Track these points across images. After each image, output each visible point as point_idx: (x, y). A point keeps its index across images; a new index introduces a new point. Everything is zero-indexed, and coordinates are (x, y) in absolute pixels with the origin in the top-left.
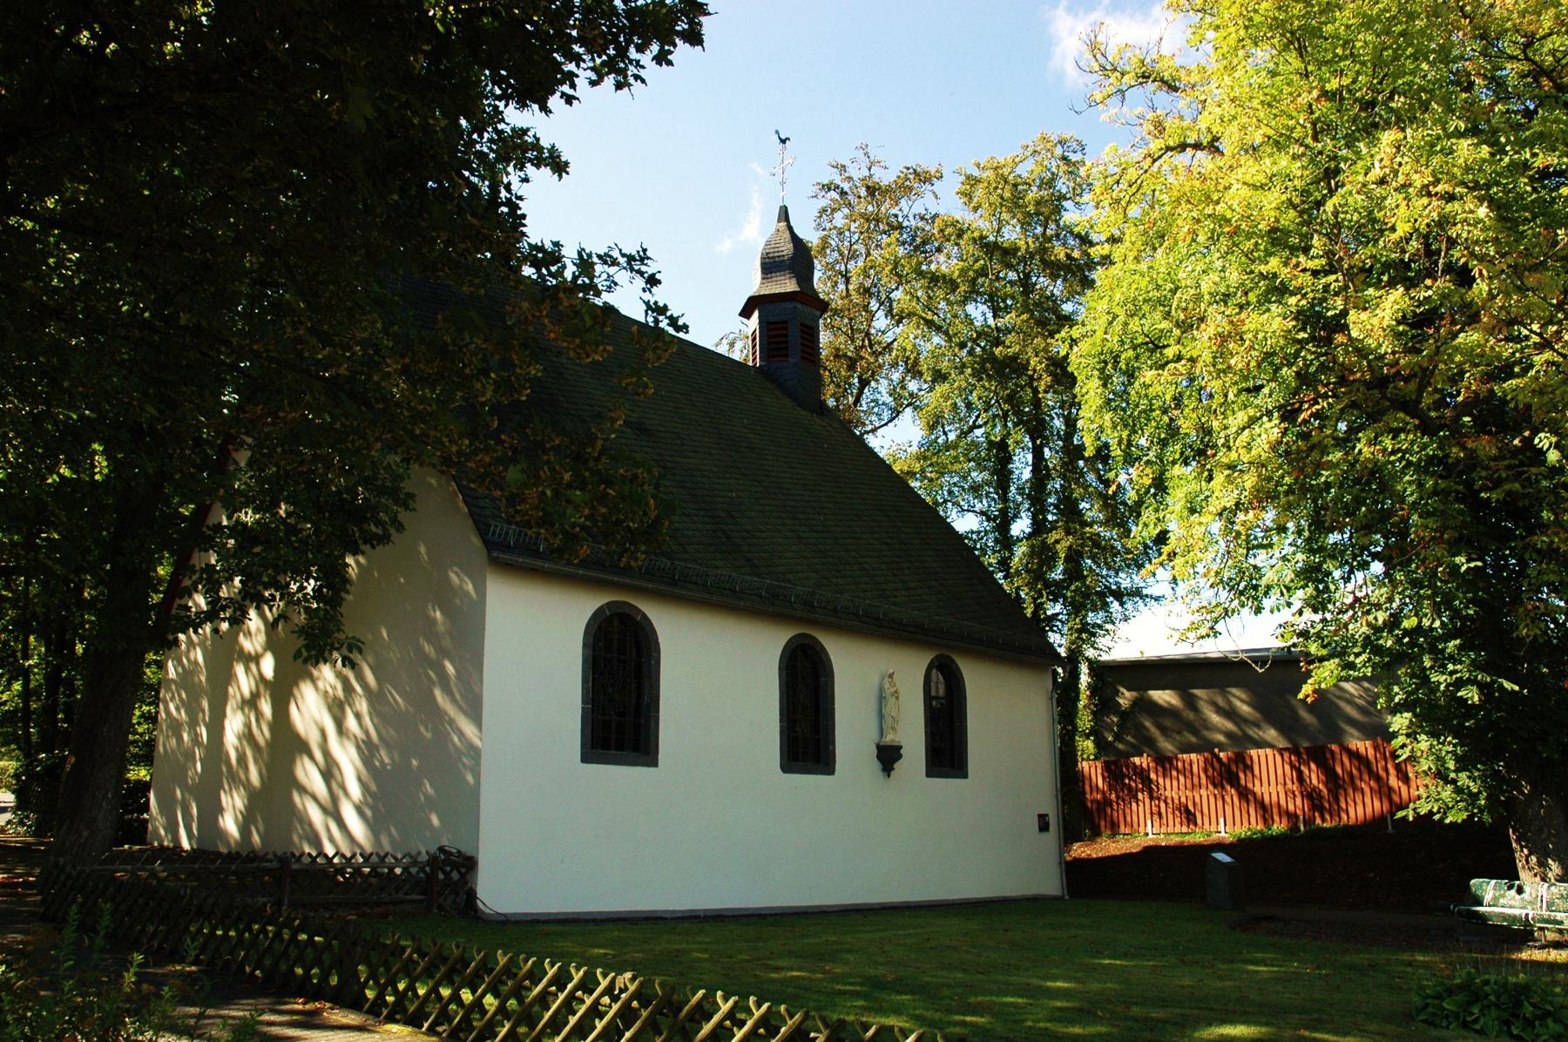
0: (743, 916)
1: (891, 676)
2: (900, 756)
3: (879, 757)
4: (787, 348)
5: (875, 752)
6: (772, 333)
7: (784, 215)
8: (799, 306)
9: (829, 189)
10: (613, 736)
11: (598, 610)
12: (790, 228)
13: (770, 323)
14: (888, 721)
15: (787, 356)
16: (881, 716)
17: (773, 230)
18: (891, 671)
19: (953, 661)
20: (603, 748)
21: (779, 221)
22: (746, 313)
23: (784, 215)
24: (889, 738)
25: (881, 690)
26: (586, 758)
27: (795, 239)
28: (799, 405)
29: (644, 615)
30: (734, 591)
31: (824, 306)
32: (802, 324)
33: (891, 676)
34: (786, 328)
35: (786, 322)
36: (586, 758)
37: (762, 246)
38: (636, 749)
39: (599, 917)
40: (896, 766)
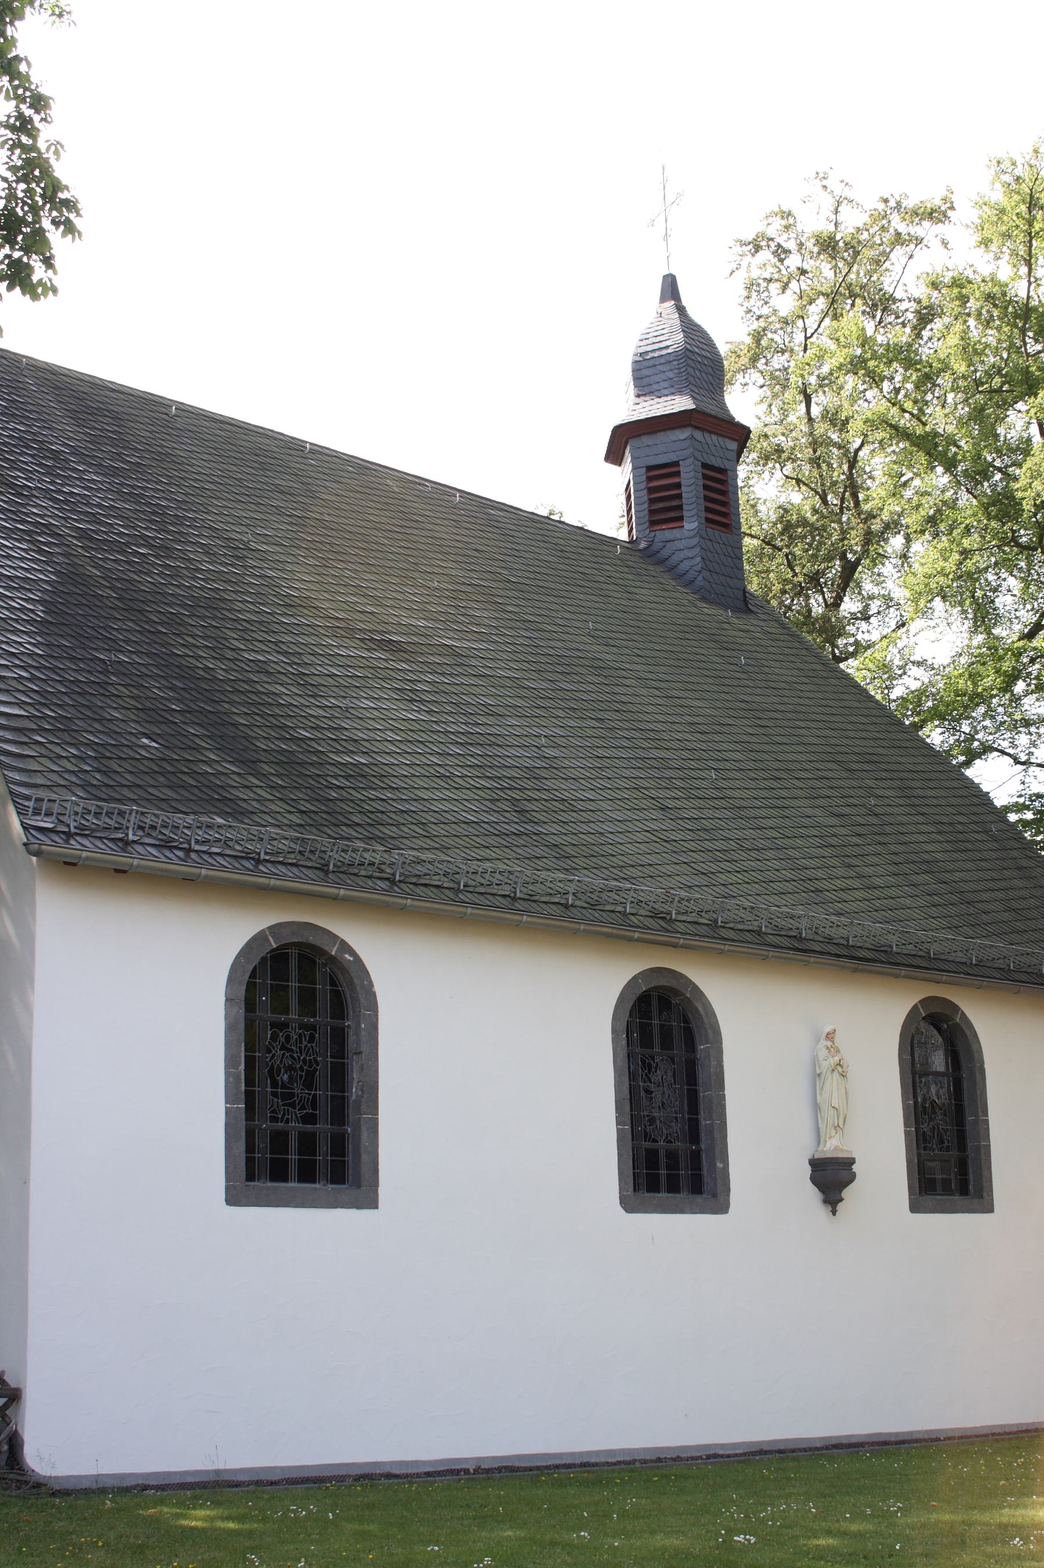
0: (557, 1467)
1: (830, 1036)
2: (852, 1177)
3: (814, 1180)
4: (680, 508)
5: (808, 1170)
6: (654, 484)
7: (670, 289)
8: (698, 434)
9: (757, 248)
10: (663, 1172)
11: (254, 939)
12: (681, 310)
13: (649, 468)
14: (829, 1116)
15: (681, 519)
16: (816, 1107)
17: (652, 316)
18: (828, 1029)
19: (956, 1008)
20: (273, 1179)
21: (663, 299)
22: (614, 455)
23: (670, 289)
24: (832, 1146)
25: (815, 1062)
26: (915, 1207)
27: (691, 329)
28: (704, 599)
29: (345, 947)
30: (392, 881)
31: (741, 435)
32: (705, 466)
33: (830, 1036)
34: (678, 474)
35: (676, 464)
36: (915, 1207)
37: (635, 342)
38: (964, 1191)
39: (264, 1477)
40: (846, 1193)
